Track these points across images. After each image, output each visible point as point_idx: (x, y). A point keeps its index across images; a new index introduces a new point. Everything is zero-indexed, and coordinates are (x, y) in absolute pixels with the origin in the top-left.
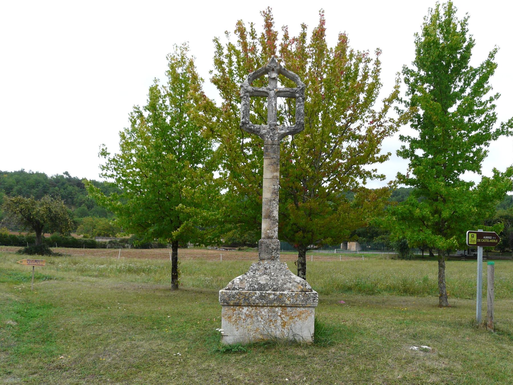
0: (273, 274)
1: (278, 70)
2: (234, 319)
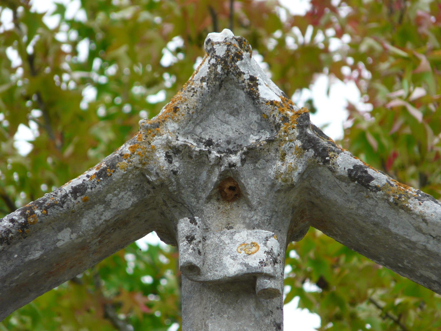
1: (282, 188)
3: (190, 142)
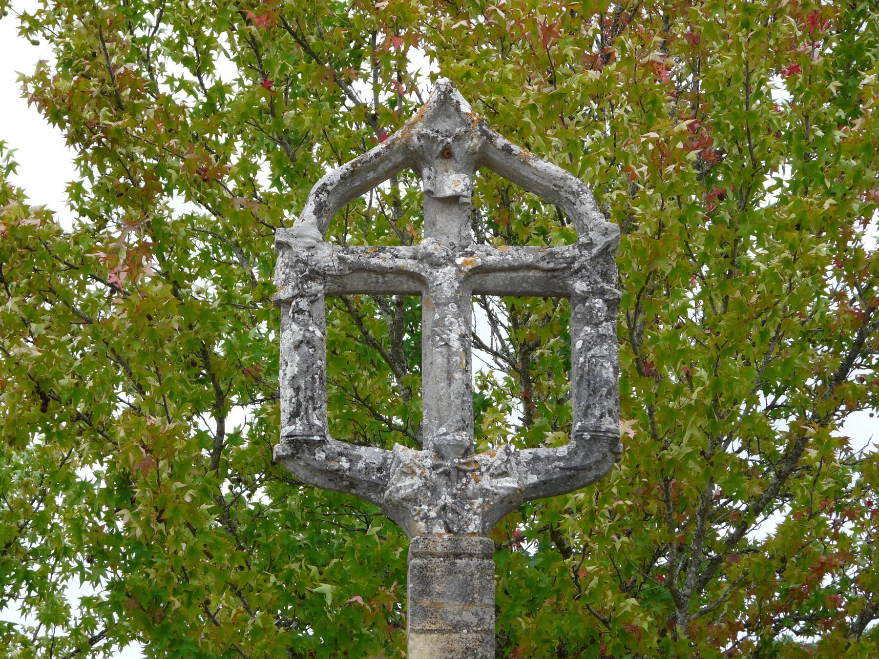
3: (429, 131)
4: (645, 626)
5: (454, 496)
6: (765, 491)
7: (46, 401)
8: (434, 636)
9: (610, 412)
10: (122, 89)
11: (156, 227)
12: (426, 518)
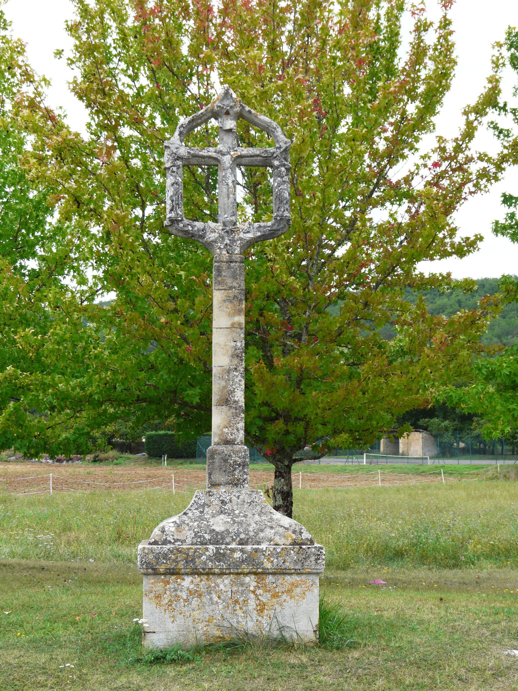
0: (237, 512)
2: (166, 601)
4: (298, 287)
5: (230, 240)
6: (342, 237)
7: (79, 204)
8: (223, 291)
9: (287, 209)
10: (105, 87)
11: (118, 139)
12: (220, 248)
